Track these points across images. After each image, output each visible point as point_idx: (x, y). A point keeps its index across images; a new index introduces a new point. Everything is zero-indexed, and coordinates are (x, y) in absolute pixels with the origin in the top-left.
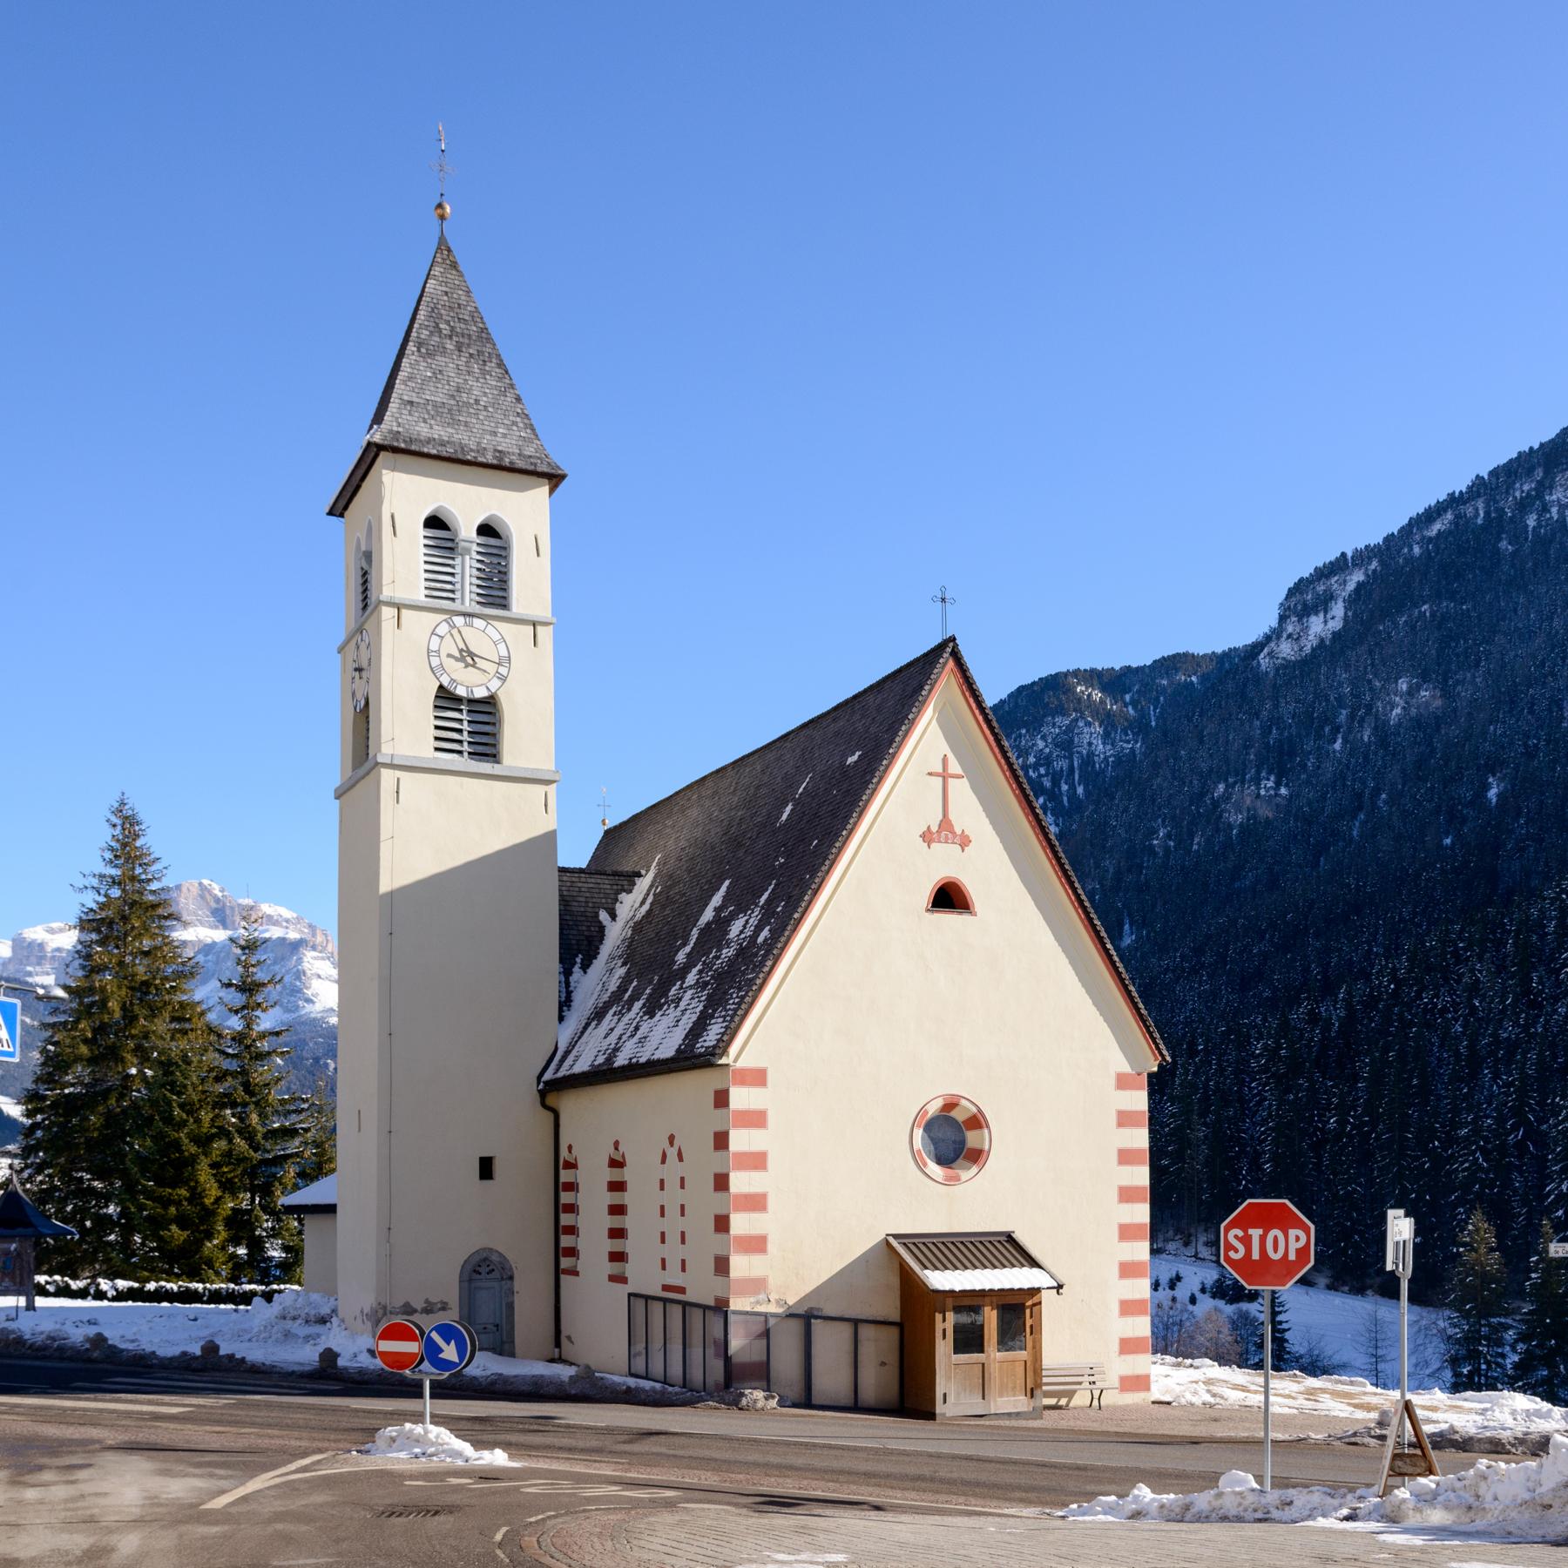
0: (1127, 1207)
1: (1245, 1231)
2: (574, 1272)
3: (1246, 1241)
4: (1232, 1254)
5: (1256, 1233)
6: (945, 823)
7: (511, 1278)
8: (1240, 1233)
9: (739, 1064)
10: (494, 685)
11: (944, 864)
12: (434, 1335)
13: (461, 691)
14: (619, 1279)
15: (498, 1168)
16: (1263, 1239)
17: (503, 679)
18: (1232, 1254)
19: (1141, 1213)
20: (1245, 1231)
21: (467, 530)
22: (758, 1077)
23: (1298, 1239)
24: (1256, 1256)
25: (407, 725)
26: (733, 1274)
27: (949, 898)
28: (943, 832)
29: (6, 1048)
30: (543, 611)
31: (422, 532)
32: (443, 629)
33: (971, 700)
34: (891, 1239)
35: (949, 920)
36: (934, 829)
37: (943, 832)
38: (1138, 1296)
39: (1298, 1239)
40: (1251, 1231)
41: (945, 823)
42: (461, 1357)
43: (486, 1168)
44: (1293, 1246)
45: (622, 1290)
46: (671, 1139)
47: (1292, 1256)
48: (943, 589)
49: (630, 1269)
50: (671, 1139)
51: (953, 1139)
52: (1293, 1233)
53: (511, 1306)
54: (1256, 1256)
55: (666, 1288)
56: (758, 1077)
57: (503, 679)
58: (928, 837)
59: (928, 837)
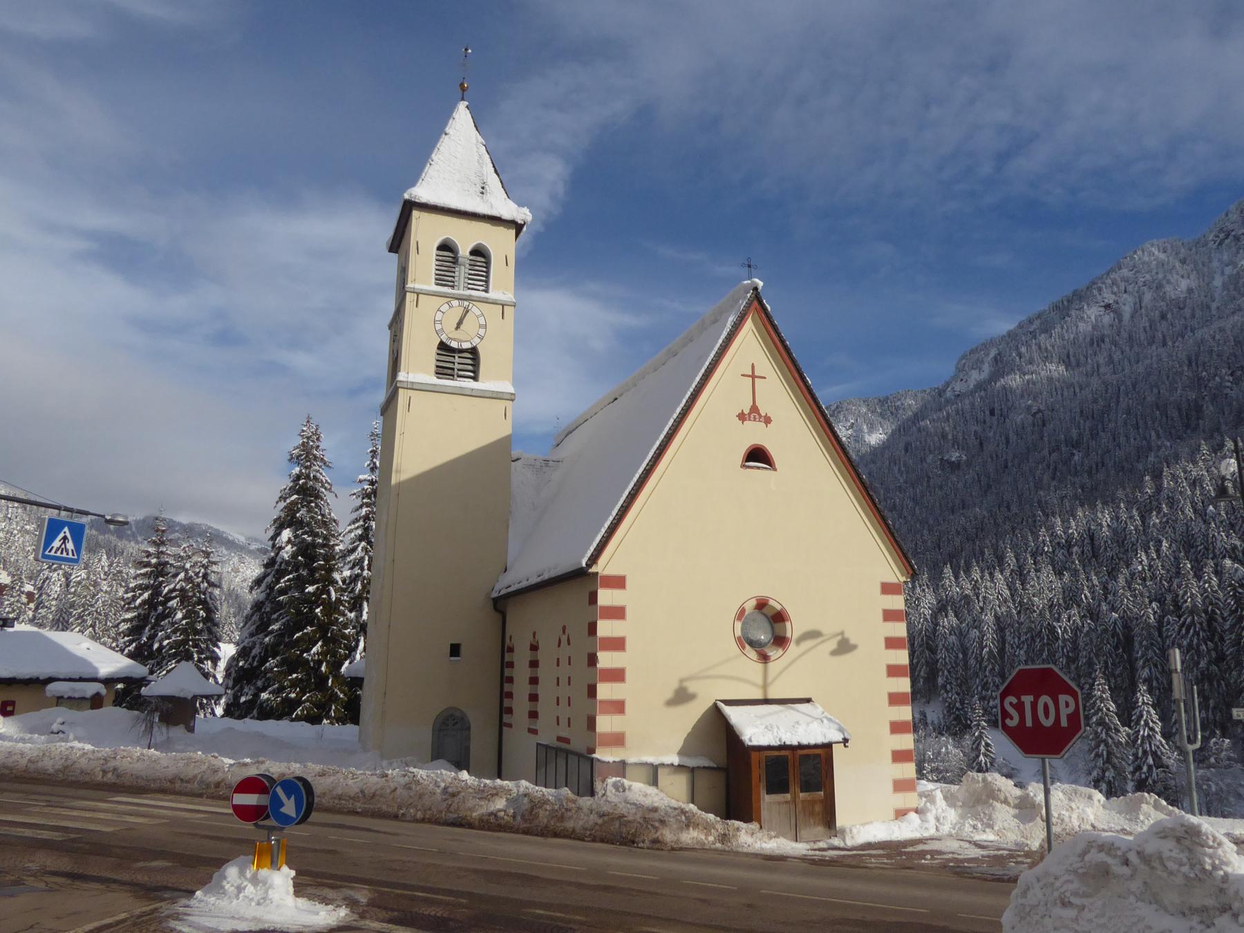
0: (894, 680)
1: (1019, 699)
2: (510, 726)
3: (1020, 707)
4: (1008, 721)
5: (1027, 700)
6: (754, 409)
7: (469, 728)
8: (1014, 700)
9: (606, 572)
10: (476, 341)
11: (755, 434)
12: (279, 790)
13: (454, 345)
14: (533, 732)
15: (463, 650)
16: (1034, 706)
17: (482, 338)
18: (1008, 721)
19: (904, 685)
20: (1019, 699)
21: (464, 251)
22: (618, 582)
23: (1067, 705)
24: (1029, 723)
25: (418, 367)
26: (599, 729)
27: (757, 455)
28: (753, 414)
29: (70, 556)
30: (509, 296)
31: (434, 251)
32: (445, 308)
33: (769, 327)
34: (722, 705)
35: (758, 473)
36: (747, 411)
37: (753, 414)
38: (904, 747)
39: (1067, 705)
40: (1023, 698)
41: (754, 409)
42: (298, 812)
43: (455, 650)
44: (1065, 712)
45: (534, 739)
46: (564, 629)
47: (1064, 723)
48: (749, 259)
49: (539, 724)
50: (564, 629)
51: (768, 627)
52: (1063, 698)
53: (468, 749)
54: (1029, 723)
55: (560, 739)
56: (618, 582)
57: (482, 338)
58: (742, 417)
59: (742, 417)
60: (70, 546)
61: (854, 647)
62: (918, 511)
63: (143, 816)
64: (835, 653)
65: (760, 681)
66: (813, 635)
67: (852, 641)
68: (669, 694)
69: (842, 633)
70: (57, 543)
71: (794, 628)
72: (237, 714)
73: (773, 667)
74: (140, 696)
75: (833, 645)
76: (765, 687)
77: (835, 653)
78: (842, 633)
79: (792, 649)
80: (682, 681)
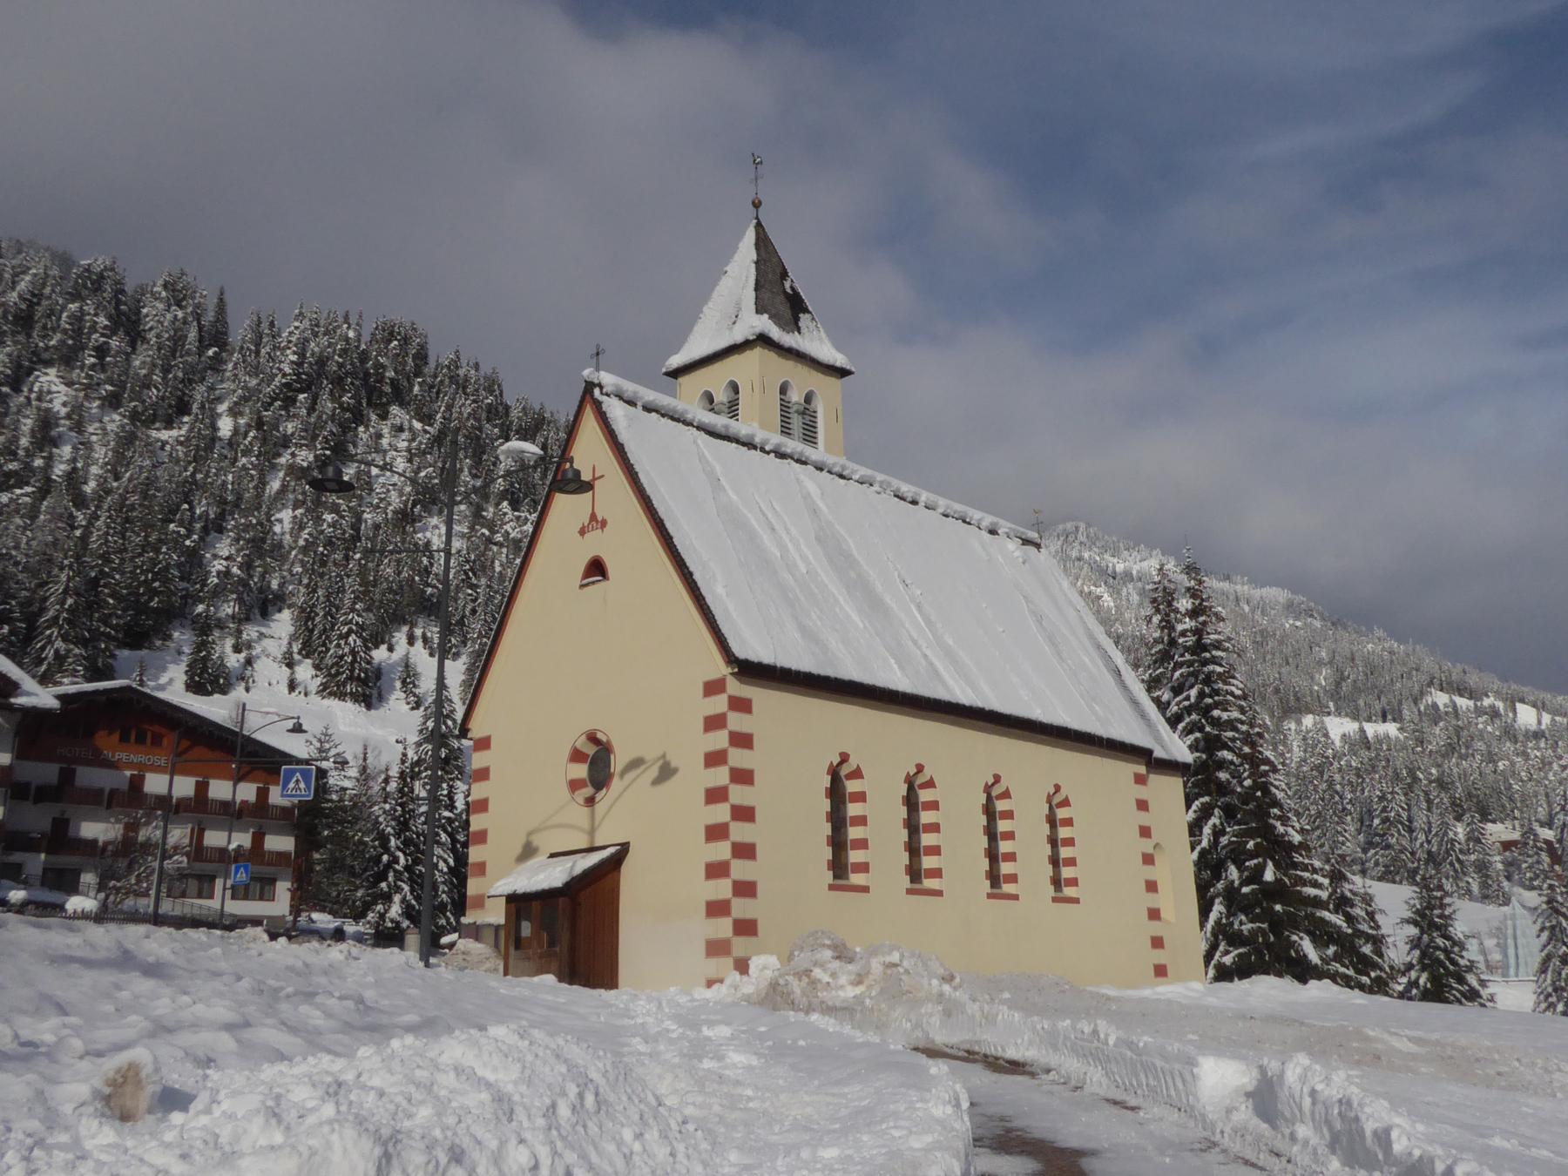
60: (302, 785)
61: (675, 771)
62: (425, 560)
63: (834, 1095)
64: (658, 781)
65: (586, 825)
66: (636, 763)
67: (673, 764)
68: (519, 850)
69: (664, 756)
70: (291, 785)
71: (618, 761)
72: (110, 848)
73: (600, 807)
74: (1192, 1063)
75: (654, 772)
76: (592, 832)
77: (658, 781)
78: (664, 756)
79: (616, 784)
80: (529, 834)
